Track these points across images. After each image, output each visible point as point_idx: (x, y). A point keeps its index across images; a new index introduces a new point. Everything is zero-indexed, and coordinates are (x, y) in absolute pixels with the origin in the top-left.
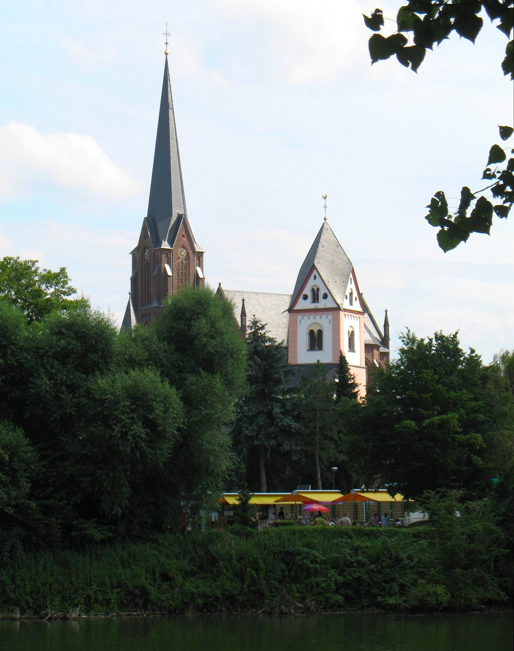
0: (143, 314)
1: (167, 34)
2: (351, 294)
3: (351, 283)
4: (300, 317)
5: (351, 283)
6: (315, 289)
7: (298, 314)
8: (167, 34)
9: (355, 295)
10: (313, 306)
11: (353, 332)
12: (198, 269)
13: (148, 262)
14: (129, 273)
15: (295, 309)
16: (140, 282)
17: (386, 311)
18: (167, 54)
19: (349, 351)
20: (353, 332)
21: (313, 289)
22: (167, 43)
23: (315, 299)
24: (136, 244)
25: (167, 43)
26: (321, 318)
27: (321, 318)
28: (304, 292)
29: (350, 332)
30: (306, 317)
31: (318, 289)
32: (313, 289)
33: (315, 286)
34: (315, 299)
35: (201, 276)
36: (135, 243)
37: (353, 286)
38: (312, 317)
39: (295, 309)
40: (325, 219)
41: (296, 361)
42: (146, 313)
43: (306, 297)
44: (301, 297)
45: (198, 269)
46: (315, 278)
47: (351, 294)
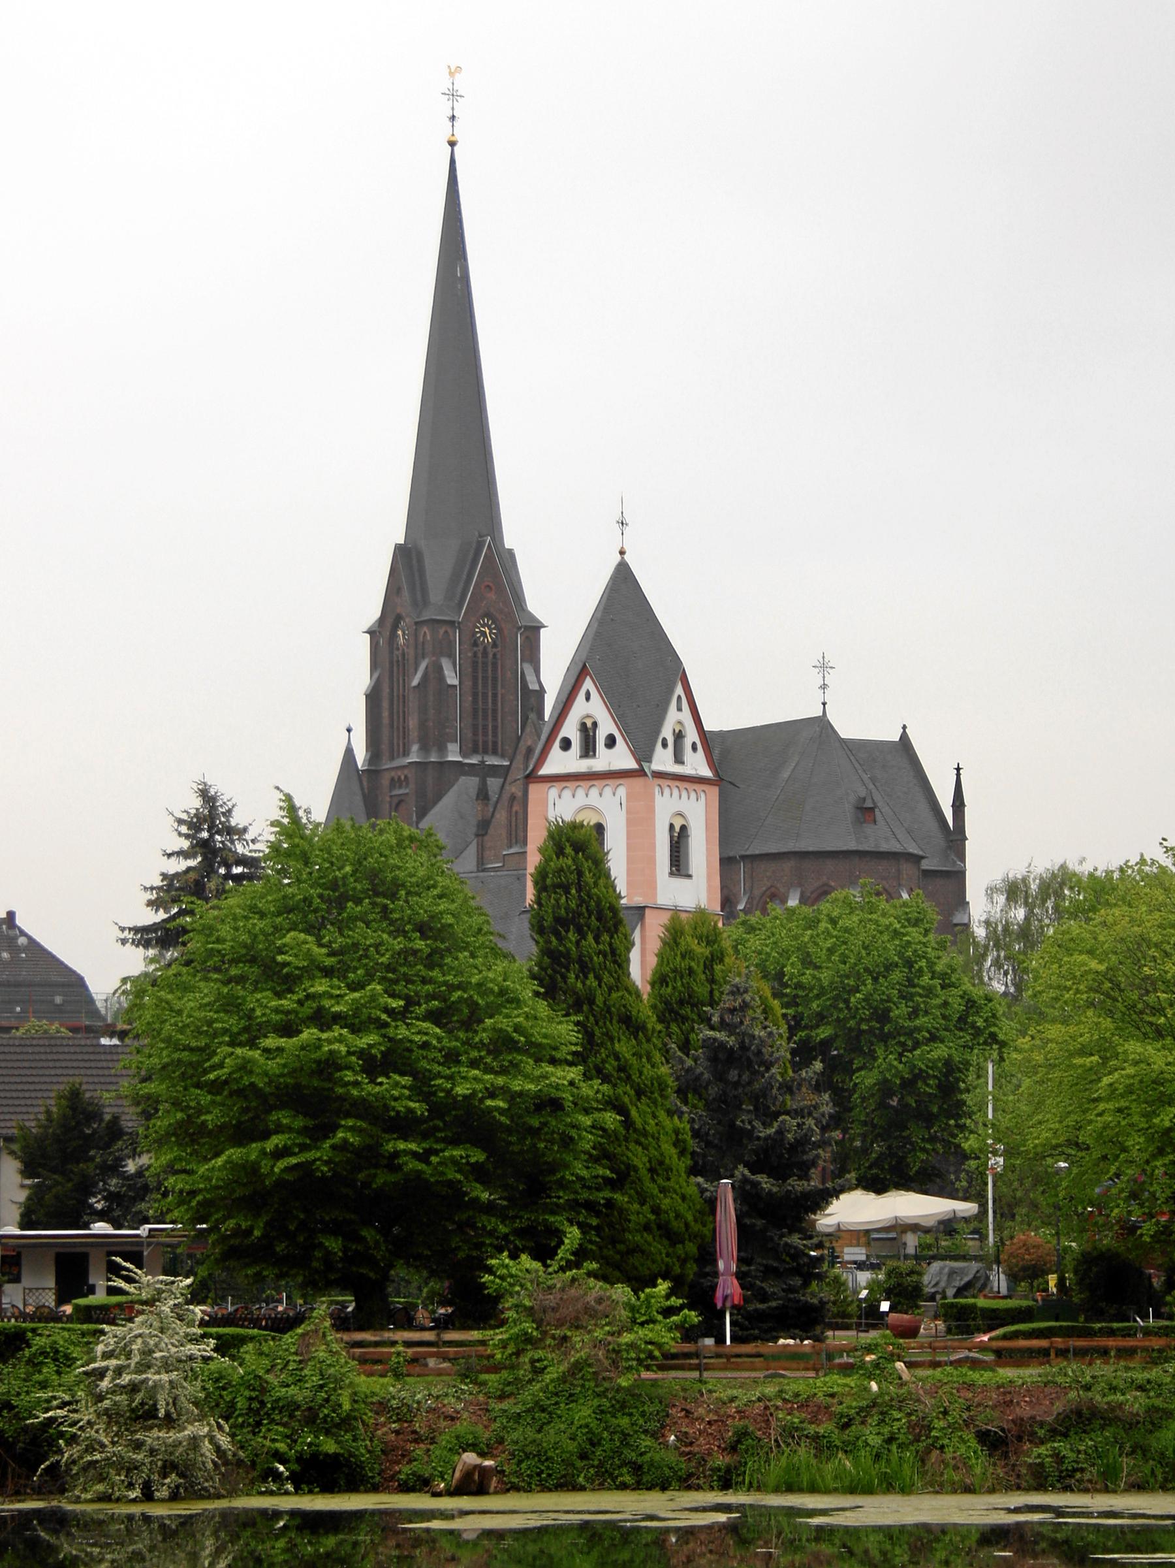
0: (392, 779)
1: (453, 95)
2: (679, 736)
3: (679, 709)
4: (553, 792)
5: (679, 709)
6: (589, 725)
7: (549, 785)
8: (453, 95)
9: (692, 736)
10: (584, 766)
11: (684, 828)
12: (529, 670)
13: (403, 654)
14: (362, 679)
15: (542, 772)
16: (385, 704)
17: (958, 769)
18: (452, 144)
19: (671, 874)
20: (684, 828)
21: (584, 725)
22: (453, 118)
23: (588, 749)
24: (376, 613)
25: (453, 118)
26: (601, 795)
27: (601, 795)
28: (562, 734)
29: (677, 829)
30: (567, 794)
31: (595, 724)
32: (584, 725)
33: (588, 716)
34: (588, 749)
35: (534, 686)
36: (373, 611)
37: (686, 716)
38: (580, 792)
39: (542, 772)
40: (622, 553)
41: (655, 895)
42: (399, 778)
43: (566, 744)
44: (557, 744)
45: (529, 670)
46: (588, 698)
47: (679, 736)
